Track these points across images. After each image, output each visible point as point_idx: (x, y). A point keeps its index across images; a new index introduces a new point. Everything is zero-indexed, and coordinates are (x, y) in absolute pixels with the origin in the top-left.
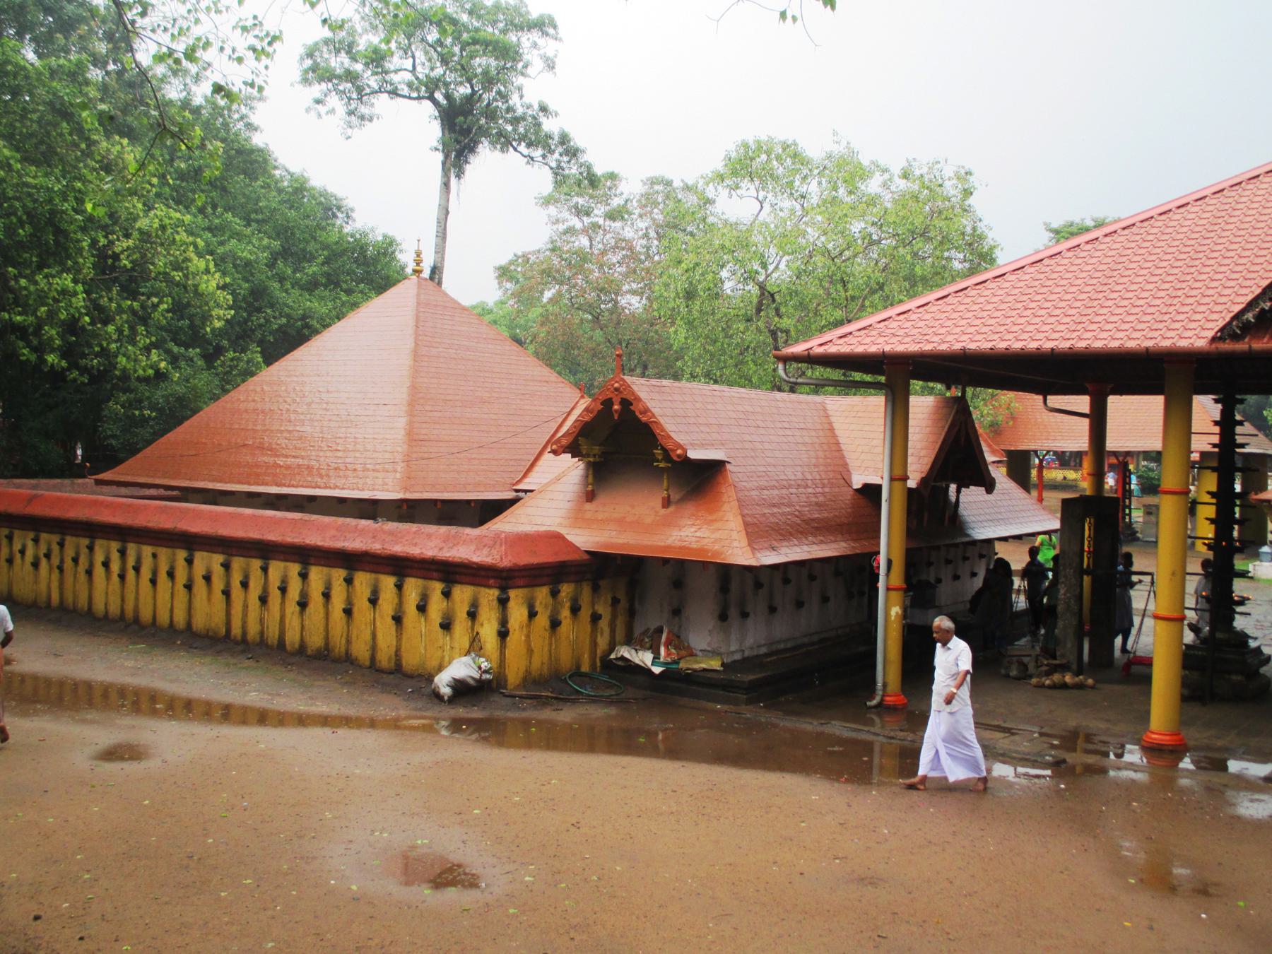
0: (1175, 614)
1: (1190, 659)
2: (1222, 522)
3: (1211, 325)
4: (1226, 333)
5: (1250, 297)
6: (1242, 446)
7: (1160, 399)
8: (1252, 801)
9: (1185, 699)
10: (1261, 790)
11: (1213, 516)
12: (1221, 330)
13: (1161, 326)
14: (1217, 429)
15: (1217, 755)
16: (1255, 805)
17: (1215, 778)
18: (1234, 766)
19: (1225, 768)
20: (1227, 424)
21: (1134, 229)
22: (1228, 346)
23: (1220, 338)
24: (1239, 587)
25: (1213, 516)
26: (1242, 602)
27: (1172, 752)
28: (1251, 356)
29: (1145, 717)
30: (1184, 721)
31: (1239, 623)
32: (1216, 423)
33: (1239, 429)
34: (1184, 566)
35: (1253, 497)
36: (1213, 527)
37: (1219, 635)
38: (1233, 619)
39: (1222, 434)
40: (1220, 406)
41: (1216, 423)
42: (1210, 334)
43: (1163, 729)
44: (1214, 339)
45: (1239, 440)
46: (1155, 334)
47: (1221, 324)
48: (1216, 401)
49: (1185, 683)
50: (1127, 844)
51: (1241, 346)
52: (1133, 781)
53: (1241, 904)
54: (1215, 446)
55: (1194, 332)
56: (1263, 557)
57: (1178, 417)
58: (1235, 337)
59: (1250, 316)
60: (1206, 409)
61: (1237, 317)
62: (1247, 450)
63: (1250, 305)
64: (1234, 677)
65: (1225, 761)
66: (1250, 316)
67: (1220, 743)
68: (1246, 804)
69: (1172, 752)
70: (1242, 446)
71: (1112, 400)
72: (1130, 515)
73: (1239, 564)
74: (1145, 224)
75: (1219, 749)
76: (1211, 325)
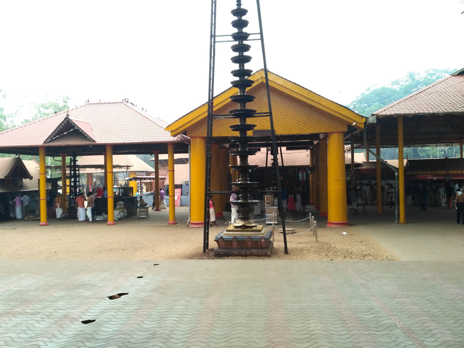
51: (47, 144)
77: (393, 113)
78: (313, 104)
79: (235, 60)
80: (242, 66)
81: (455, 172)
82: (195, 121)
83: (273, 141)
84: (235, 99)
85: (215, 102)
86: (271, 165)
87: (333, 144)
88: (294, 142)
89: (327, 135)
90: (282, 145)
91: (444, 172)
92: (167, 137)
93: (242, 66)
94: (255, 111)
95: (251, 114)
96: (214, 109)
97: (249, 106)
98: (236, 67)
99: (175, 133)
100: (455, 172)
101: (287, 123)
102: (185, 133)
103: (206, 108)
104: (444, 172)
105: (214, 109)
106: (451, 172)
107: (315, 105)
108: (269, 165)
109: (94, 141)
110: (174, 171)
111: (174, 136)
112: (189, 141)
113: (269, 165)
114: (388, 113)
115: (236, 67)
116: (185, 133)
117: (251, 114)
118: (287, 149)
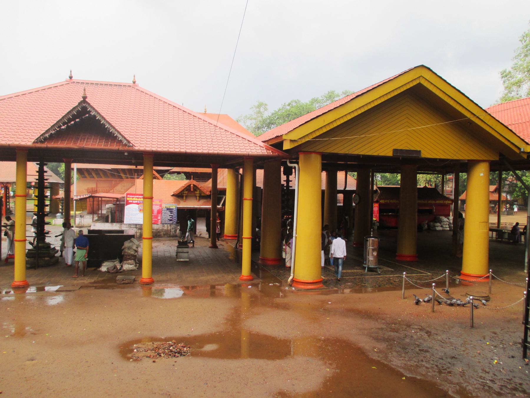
0: (22, 239)
1: (29, 254)
2: (41, 205)
3: (33, 137)
4: (38, 141)
5: (48, 128)
6: (47, 180)
7: (14, 164)
8: (52, 299)
9: (27, 268)
10: (55, 295)
11: (37, 204)
12: (37, 139)
13: (15, 136)
14: (37, 174)
15: (40, 286)
16: (53, 300)
17: (41, 293)
18: (47, 288)
19: (44, 290)
20: (41, 172)
21: (5, 101)
22: (39, 145)
23: (36, 142)
24: (47, 228)
25: (37, 204)
26: (48, 233)
27: (23, 287)
28: (47, 149)
29: (13, 277)
30: (27, 276)
31: (47, 240)
32: (37, 172)
33: (45, 174)
34: (25, 222)
35: (54, 197)
36: (37, 208)
37: (40, 245)
38: (45, 239)
39: (39, 176)
40: (38, 166)
41: (37, 172)
42: (33, 140)
43: (19, 280)
44: (34, 142)
45: (46, 178)
46: (13, 139)
47: (37, 137)
48: (37, 164)
49: (27, 263)
50: (5, 324)
51: (44, 145)
52: (8, 300)
53: (47, 334)
54: (37, 180)
55: (27, 139)
56: (57, 217)
57: (22, 170)
58: (41, 142)
59: (47, 135)
60: (32, 167)
61: (42, 135)
62: (48, 181)
63: (47, 132)
64: (46, 259)
65: (44, 287)
66: (47, 135)
67: (41, 282)
68: (50, 301)
69: (23, 287)
70: (47, 180)
71: (219, 170)
72: (9, 205)
73: (47, 220)
74: (9, 99)
75: (42, 283)
76: (33, 137)
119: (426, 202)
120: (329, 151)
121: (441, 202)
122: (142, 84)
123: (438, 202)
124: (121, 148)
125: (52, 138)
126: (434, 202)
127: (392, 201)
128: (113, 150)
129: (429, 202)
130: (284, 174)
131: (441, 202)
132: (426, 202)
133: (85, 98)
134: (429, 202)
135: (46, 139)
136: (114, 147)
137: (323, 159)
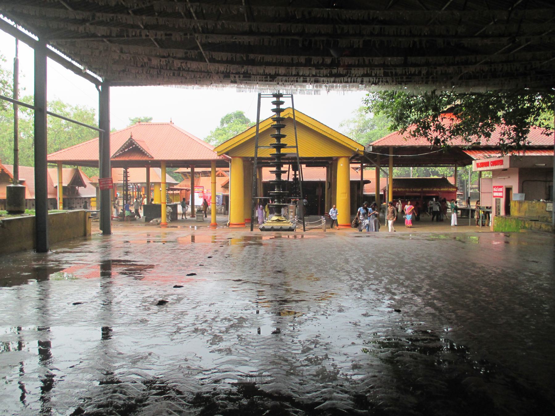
0: (349, 224)
51: (117, 159)
77: (384, 144)
78: (326, 135)
79: (274, 103)
80: (278, 150)
81: (428, 189)
82: (242, 141)
83: (296, 163)
84: (274, 127)
85: (260, 127)
86: (292, 180)
87: (341, 165)
88: (313, 162)
89: (336, 159)
90: (302, 163)
91: (419, 190)
92: (214, 156)
93: (278, 150)
94: (286, 145)
95: (284, 146)
96: (259, 132)
97: (283, 141)
98: (275, 107)
99: (220, 154)
100: (428, 189)
101: (308, 148)
102: (227, 153)
103: (254, 129)
104: (419, 190)
105: (259, 132)
106: (425, 189)
107: (328, 136)
108: (291, 180)
109: (152, 158)
110: (215, 183)
111: (219, 156)
112: (230, 160)
113: (291, 180)
114: (380, 144)
115: (275, 107)
116: (227, 153)
117: (284, 146)
118: (306, 166)
119: (431, 189)
120: (244, 156)
121: (446, 189)
122: (177, 124)
123: (442, 189)
124: (147, 159)
125: (120, 155)
126: (438, 190)
127: (399, 190)
128: (544, 151)
129: (434, 190)
130: (293, 170)
131: (446, 189)
132: (431, 189)
133: (131, 136)
134: (434, 190)
135: (116, 157)
136: (145, 159)
137: (244, 161)
